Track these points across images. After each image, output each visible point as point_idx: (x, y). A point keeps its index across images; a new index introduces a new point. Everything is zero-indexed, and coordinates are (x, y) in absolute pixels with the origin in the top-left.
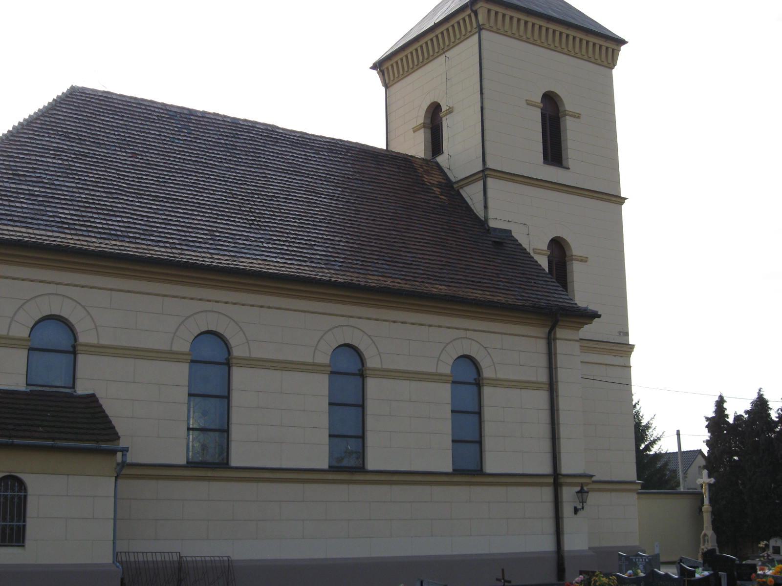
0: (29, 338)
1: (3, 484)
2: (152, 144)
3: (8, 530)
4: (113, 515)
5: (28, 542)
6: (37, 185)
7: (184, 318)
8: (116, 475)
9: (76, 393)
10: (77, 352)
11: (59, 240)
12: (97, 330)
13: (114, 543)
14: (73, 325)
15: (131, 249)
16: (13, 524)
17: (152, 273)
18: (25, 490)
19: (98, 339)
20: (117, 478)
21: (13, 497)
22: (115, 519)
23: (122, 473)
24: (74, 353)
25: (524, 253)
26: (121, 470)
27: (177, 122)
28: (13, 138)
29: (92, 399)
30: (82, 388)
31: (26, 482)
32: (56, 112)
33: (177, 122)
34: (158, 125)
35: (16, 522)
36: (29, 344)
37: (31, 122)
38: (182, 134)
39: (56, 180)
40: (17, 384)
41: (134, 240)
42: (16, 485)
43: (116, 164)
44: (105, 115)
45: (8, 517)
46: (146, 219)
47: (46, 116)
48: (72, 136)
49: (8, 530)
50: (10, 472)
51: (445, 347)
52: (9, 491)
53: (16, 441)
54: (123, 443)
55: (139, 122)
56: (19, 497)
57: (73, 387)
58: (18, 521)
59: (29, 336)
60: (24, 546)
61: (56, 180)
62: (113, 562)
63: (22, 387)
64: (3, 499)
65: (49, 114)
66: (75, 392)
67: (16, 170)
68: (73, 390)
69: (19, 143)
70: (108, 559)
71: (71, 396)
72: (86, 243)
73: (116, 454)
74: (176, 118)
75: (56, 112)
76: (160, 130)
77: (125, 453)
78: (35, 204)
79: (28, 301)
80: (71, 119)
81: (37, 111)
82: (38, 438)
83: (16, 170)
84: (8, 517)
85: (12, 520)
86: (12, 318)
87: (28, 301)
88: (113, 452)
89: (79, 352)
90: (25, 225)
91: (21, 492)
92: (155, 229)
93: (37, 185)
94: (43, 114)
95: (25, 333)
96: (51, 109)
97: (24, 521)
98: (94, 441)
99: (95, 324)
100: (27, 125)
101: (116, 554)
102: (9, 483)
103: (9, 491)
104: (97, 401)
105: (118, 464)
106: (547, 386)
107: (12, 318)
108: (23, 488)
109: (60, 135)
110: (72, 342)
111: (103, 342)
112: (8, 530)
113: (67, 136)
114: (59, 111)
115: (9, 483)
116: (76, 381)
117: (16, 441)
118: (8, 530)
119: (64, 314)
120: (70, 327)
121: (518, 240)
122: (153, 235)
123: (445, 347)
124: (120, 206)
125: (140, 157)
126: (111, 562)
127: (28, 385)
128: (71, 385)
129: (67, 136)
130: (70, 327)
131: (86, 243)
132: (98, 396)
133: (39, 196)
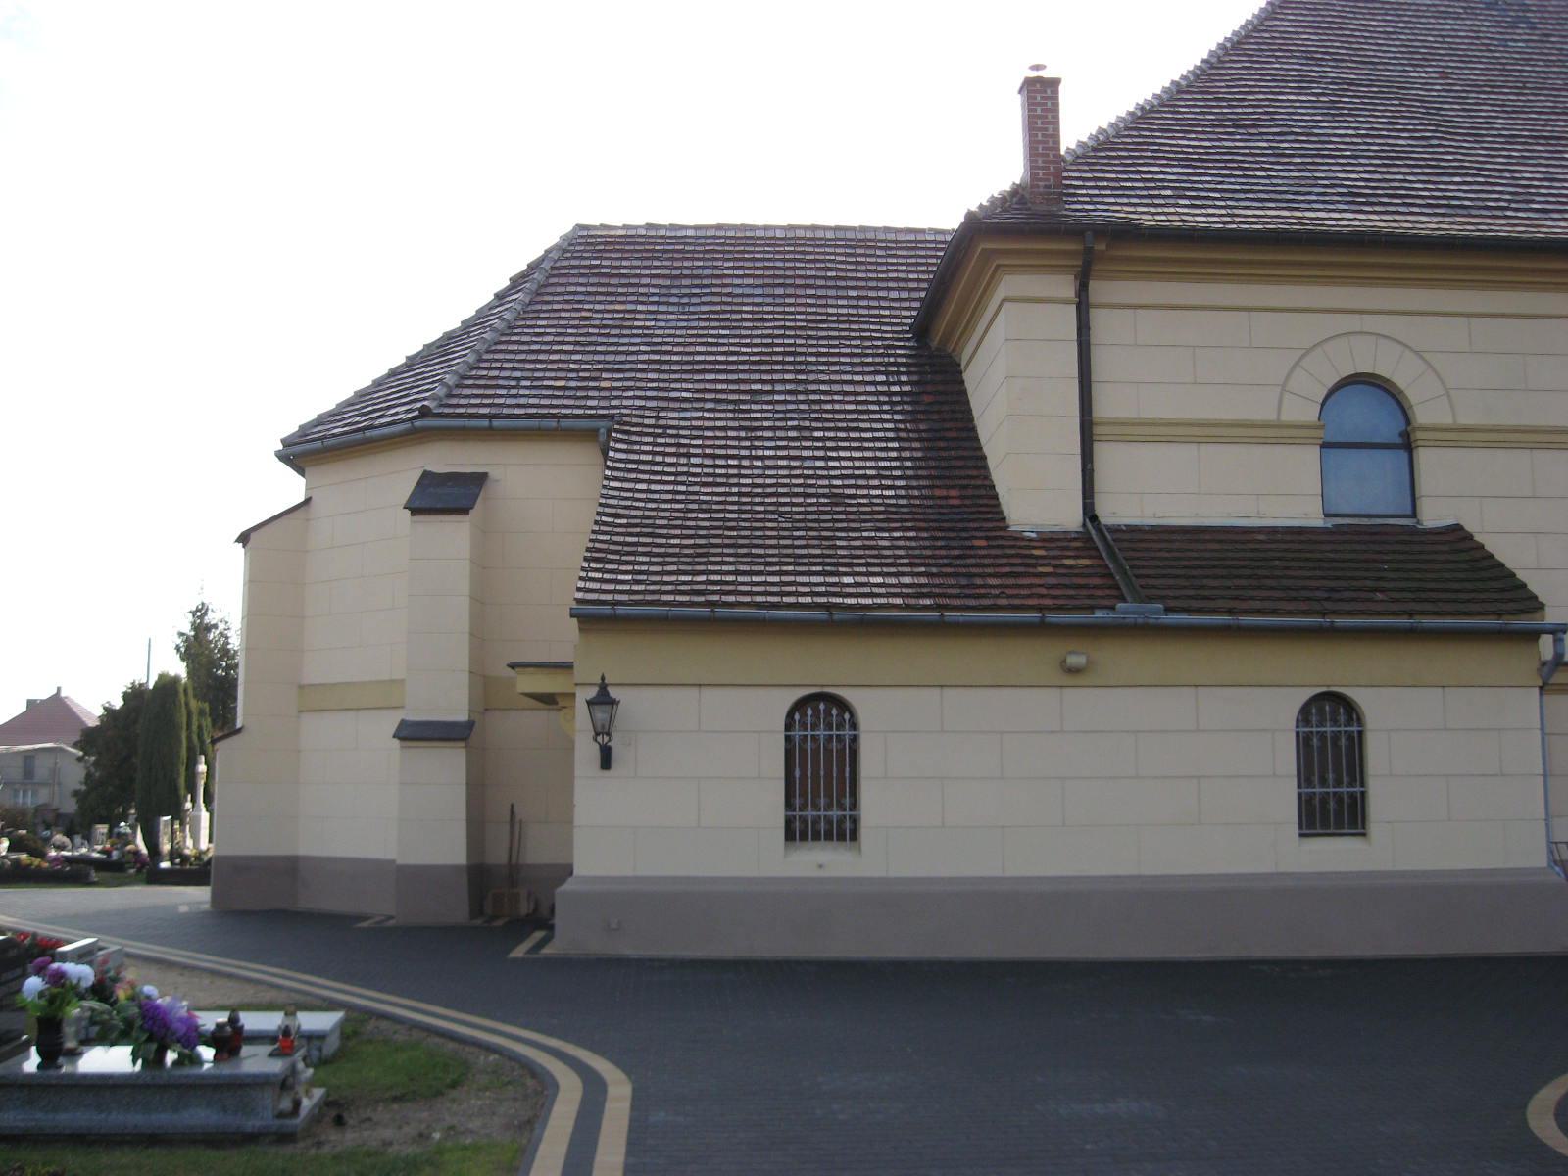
0: (1322, 423)
1: (1314, 711)
2: (1470, 53)
3: (1332, 804)
4: (1541, 766)
5: (1375, 826)
6: (1282, 138)
7: (1304, 351)
8: (1540, 684)
9: (1422, 525)
10: (1413, 445)
11: (1358, 224)
12: (1449, 396)
13: (1547, 825)
14: (1401, 392)
15: (1500, 228)
16: (1341, 790)
17: (1250, 263)
18: (1360, 721)
19: (1454, 416)
20: (1541, 688)
21: (1336, 736)
22: (1545, 776)
23: (1551, 682)
24: (1407, 444)
25: (1497, 579)
26: (1552, 672)
27: (1503, 13)
28: (1214, 71)
29: (1456, 535)
30: (1434, 515)
31: (1363, 708)
32: (1278, 23)
33: (1503, 13)
34: (1468, 22)
35: (1347, 787)
36: (1320, 433)
37: (1238, 43)
38: (1518, 31)
39: (1314, 127)
40: (1306, 514)
41: (1499, 213)
42: (1341, 710)
43: (1414, 92)
44: (1368, 16)
45: (1331, 776)
46: (1508, 175)
47: (1263, 31)
48: (1320, 56)
49: (1332, 803)
50: (1328, 686)
51: (1303, 356)
52: (1328, 724)
53: (1340, 621)
54: (1552, 616)
55: (1432, 20)
56: (1350, 736)
57: (1414, 515)
58: (1351, 784)
59: (1319, 419)
60: (1364, 835)
61: (1314, 127)
62: (1549, 865)
63: (1317, 521)
64: (1318, 740)
65: (1265, 26)
66: (1418, 523)
67: (1237, 120)
68: (1415, 521)
69: (1228, 78)
70: (1540, 860)
71: (1413, 531)
72: (1410, 226)
73: (1538, 638)
74: (1497, 7)
75: (1278, 23)
76: (1475, 29)
77: (1560, 635)
78: (1291, 170)
79: (1309, 351)
80: (1308, 31)
81: (1159, 93)
82: (1379, 614)
83: (1237, 120)
84: (1331, 776)
85: (1338, 783)
86: (1283, 387)
87: (1309, 351)
88: (1532, 636)
89: (1419, 443)
90: (1285, 205)
91: (1353, 726)
92: (1533, 191)
93: (1282, 138)
94: (1255, 28)
95: (1311, 414)
96: (1256, 30)
97: (1363, 784)
98: (1494, 613)
99: (1445, 387)
100: (1233, 48)
101: (1552, 845)
102: (1327, 708)
103: (1328, 724)
104: (1469, 537)
105: (1544, 664)
106: (1097, 430)
107: (1283, 387)
108: (1355, 717)
109: (1297, 57)
110: (1402, 427)
111: (1465, 420)
112: (1332, 803)
113: (1310, 58)
114: (1282, 19)
115: (1327, 708)
116: (1418, 503)
117: (1340, 621)
118: (1332, 804)
119: (1382, 371)
120: (1393, 396)
121: (1495, 553)
122: (1533, 202)
123: (1303, 356)
124: (1450, 157)
125: (1455, 77)
126: (1545, 865)
127: (1327, 515)
128: (1409, 512)
129: (1310, 58)
130: (1393, 396)
131: (1410, 226)
132: (1468, 528)
133: (1292, 156)
